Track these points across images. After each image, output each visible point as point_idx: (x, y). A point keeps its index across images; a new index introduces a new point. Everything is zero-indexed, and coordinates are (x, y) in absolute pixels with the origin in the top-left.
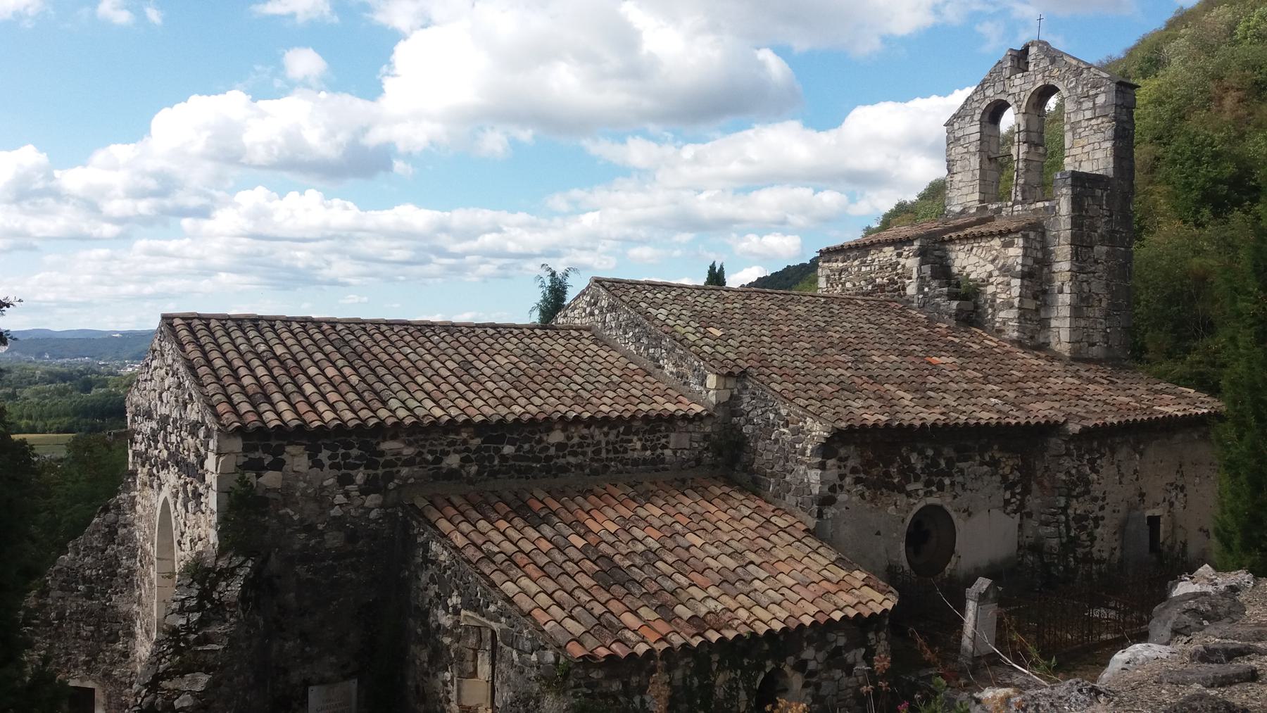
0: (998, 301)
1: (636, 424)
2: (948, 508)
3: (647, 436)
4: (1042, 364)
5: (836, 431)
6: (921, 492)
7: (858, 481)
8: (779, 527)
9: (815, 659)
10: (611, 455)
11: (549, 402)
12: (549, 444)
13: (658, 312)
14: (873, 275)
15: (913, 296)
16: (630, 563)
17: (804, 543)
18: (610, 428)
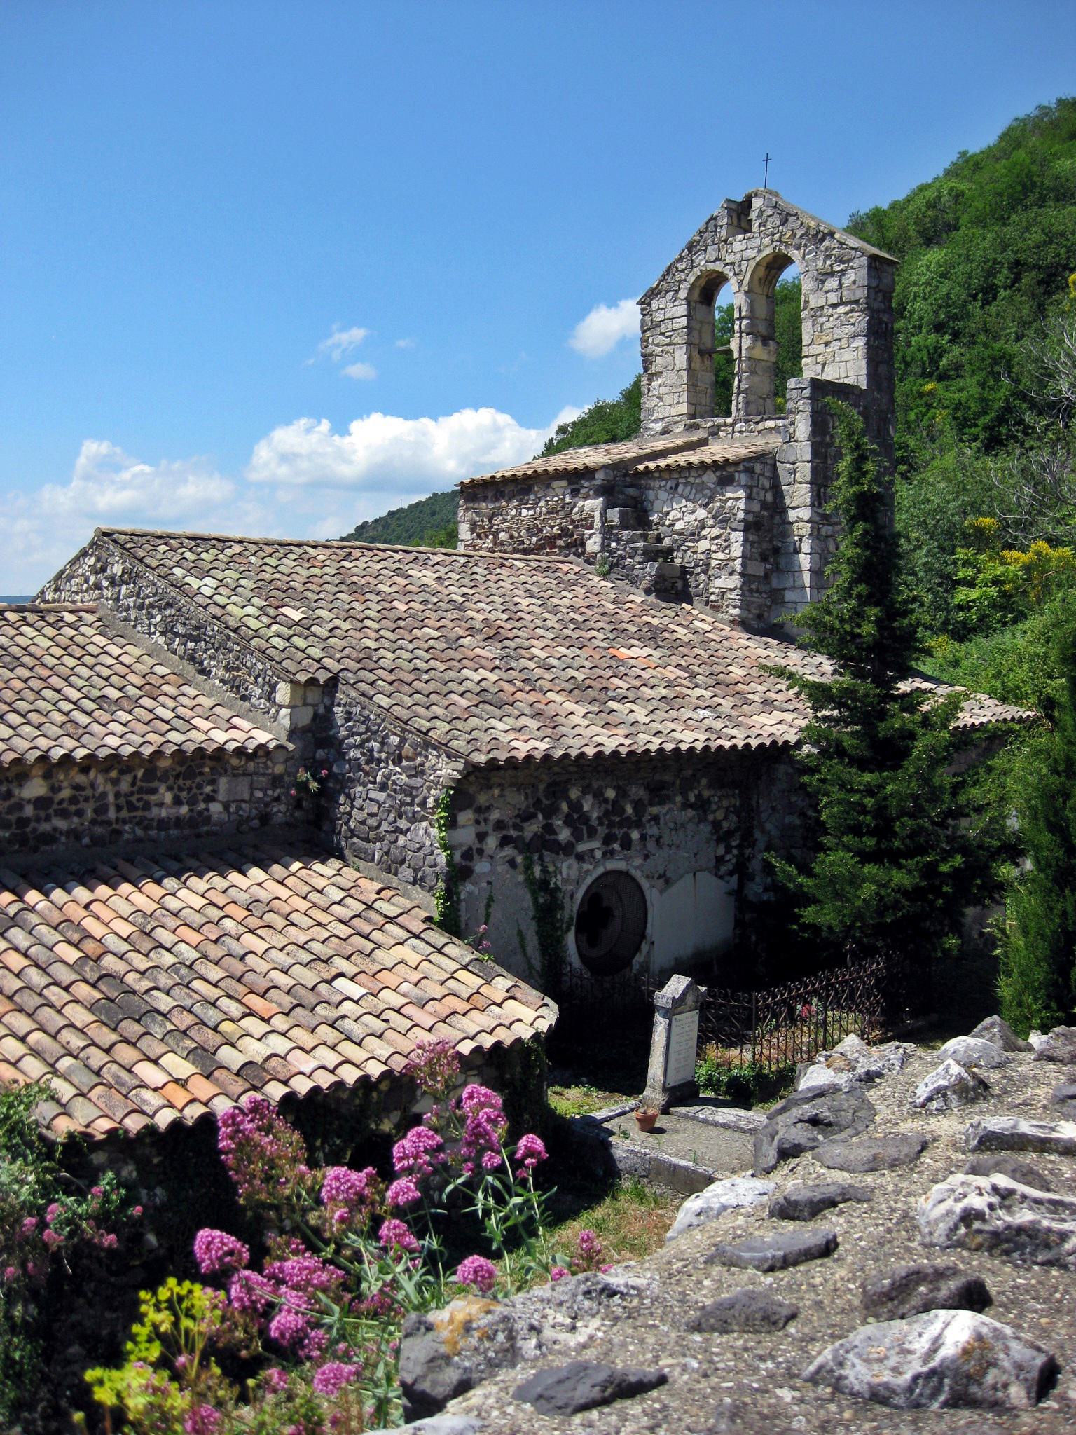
0: (714, 563)
1: (164, 764)
2: (637, 874)
3: (181, 782)
4: (773, 655)
5: (471, 769)
6: (598, 854)
7: (505, 841)
8: (387, 917)
10: (124, 814)
11: (22, 733)
12: (22, 799)
13: (202, 583)
16: (151, 985)
17: (423, 940)
18: (122, 772)
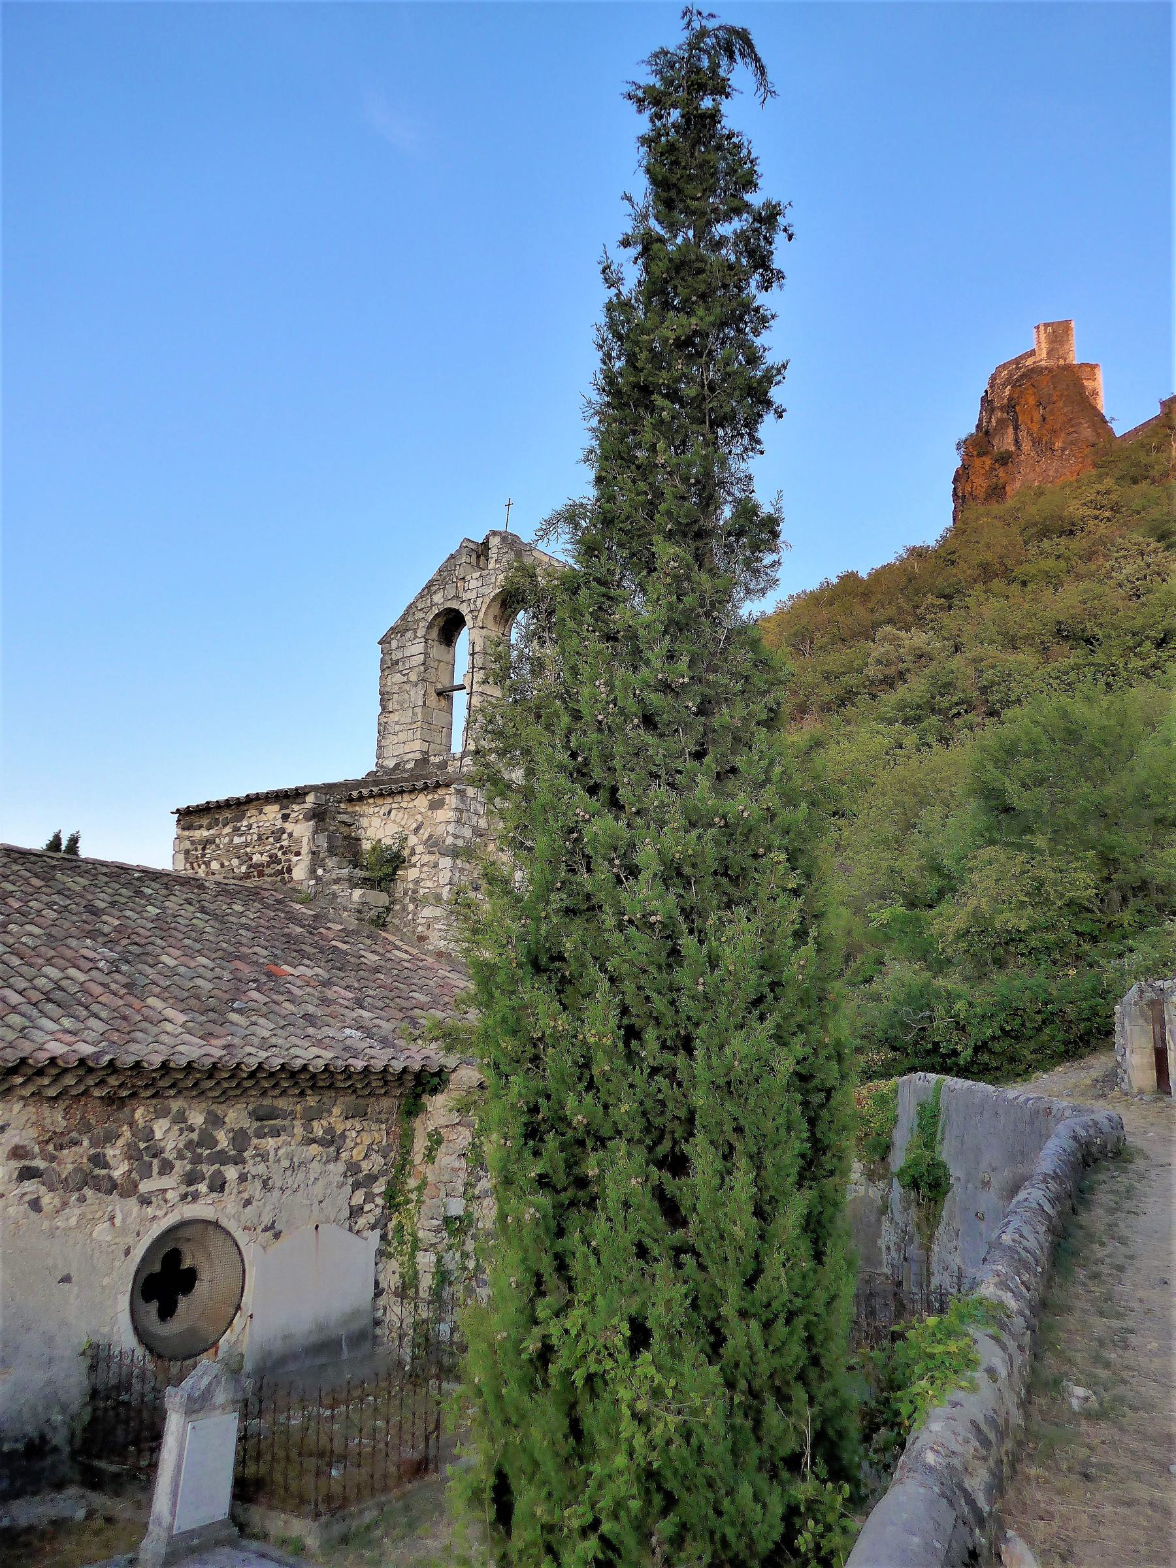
0: (422, 891)
14: (248, 850)
15: (301, 882)
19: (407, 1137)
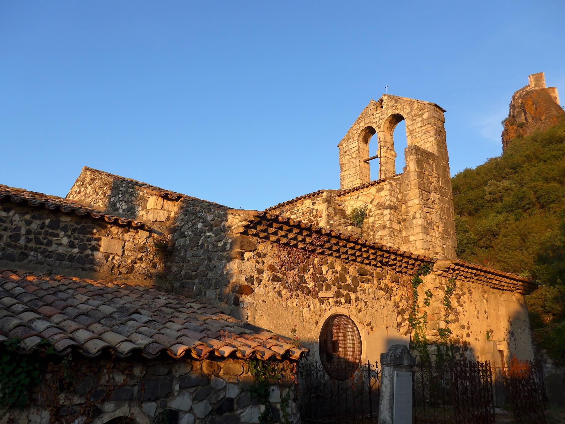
0: (376, 226)
3: (76, 235)
7: (275, 279)
9: (191, 410)
18: (34, 217)
19: (415, 294)
